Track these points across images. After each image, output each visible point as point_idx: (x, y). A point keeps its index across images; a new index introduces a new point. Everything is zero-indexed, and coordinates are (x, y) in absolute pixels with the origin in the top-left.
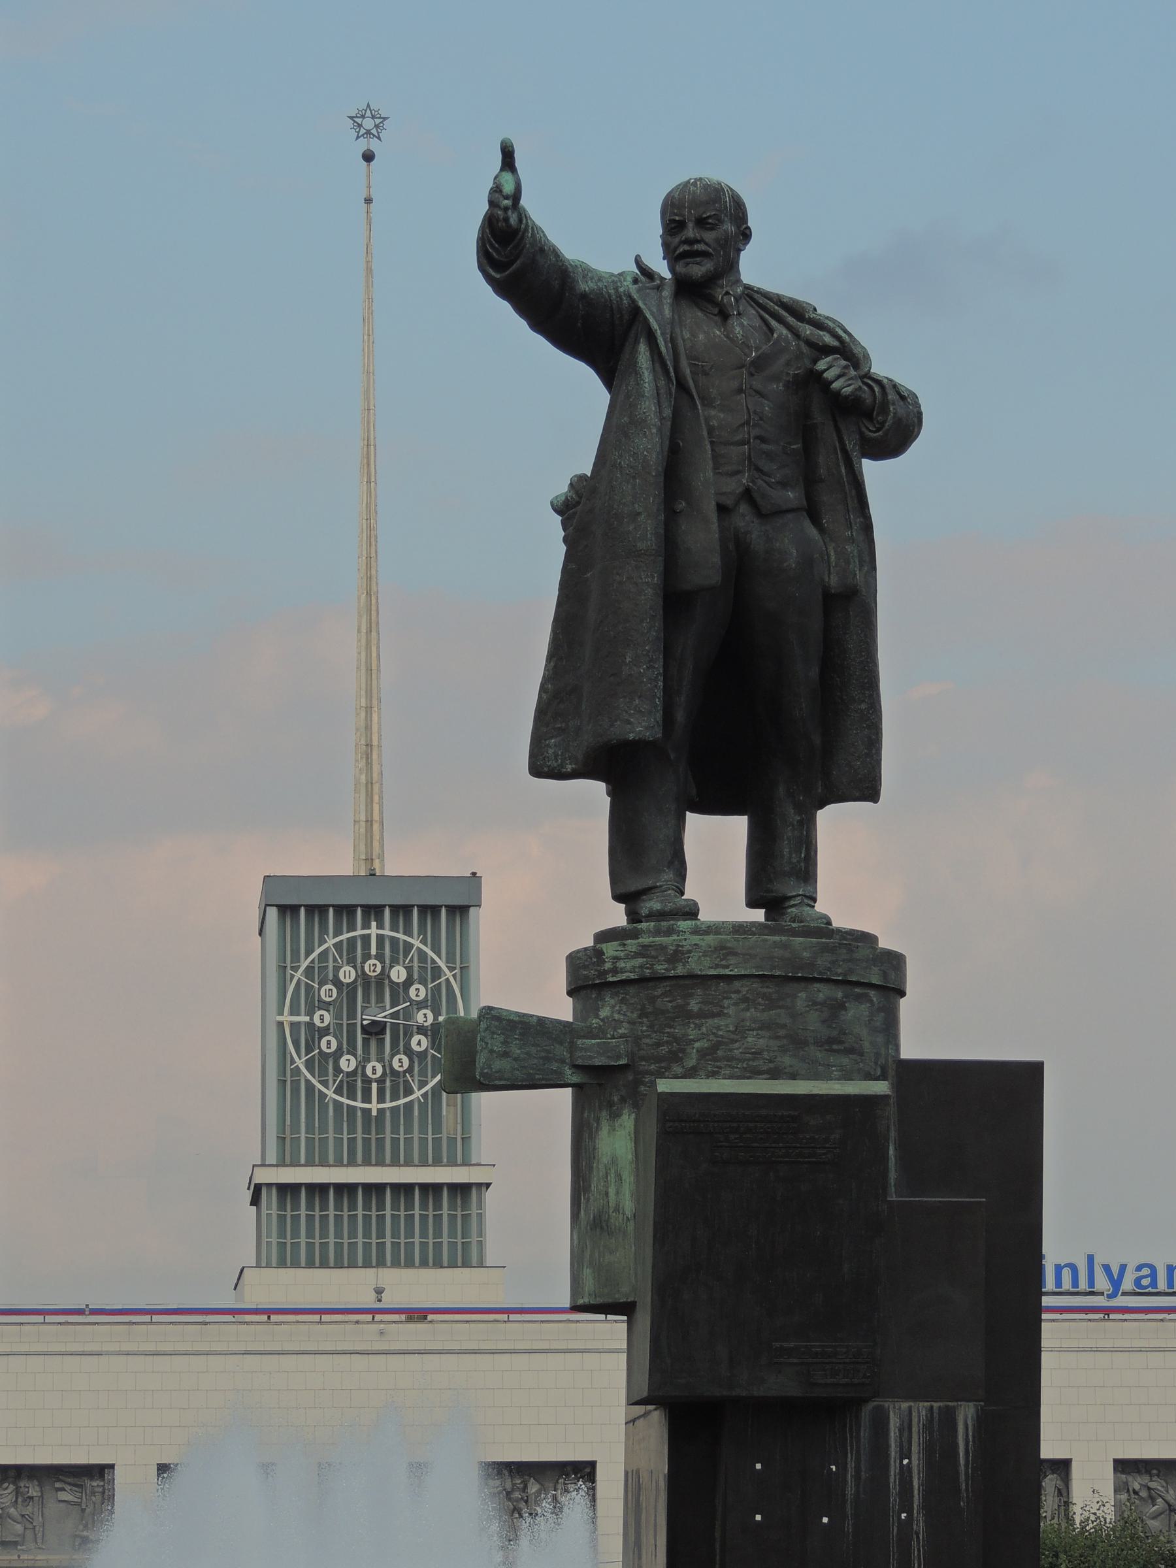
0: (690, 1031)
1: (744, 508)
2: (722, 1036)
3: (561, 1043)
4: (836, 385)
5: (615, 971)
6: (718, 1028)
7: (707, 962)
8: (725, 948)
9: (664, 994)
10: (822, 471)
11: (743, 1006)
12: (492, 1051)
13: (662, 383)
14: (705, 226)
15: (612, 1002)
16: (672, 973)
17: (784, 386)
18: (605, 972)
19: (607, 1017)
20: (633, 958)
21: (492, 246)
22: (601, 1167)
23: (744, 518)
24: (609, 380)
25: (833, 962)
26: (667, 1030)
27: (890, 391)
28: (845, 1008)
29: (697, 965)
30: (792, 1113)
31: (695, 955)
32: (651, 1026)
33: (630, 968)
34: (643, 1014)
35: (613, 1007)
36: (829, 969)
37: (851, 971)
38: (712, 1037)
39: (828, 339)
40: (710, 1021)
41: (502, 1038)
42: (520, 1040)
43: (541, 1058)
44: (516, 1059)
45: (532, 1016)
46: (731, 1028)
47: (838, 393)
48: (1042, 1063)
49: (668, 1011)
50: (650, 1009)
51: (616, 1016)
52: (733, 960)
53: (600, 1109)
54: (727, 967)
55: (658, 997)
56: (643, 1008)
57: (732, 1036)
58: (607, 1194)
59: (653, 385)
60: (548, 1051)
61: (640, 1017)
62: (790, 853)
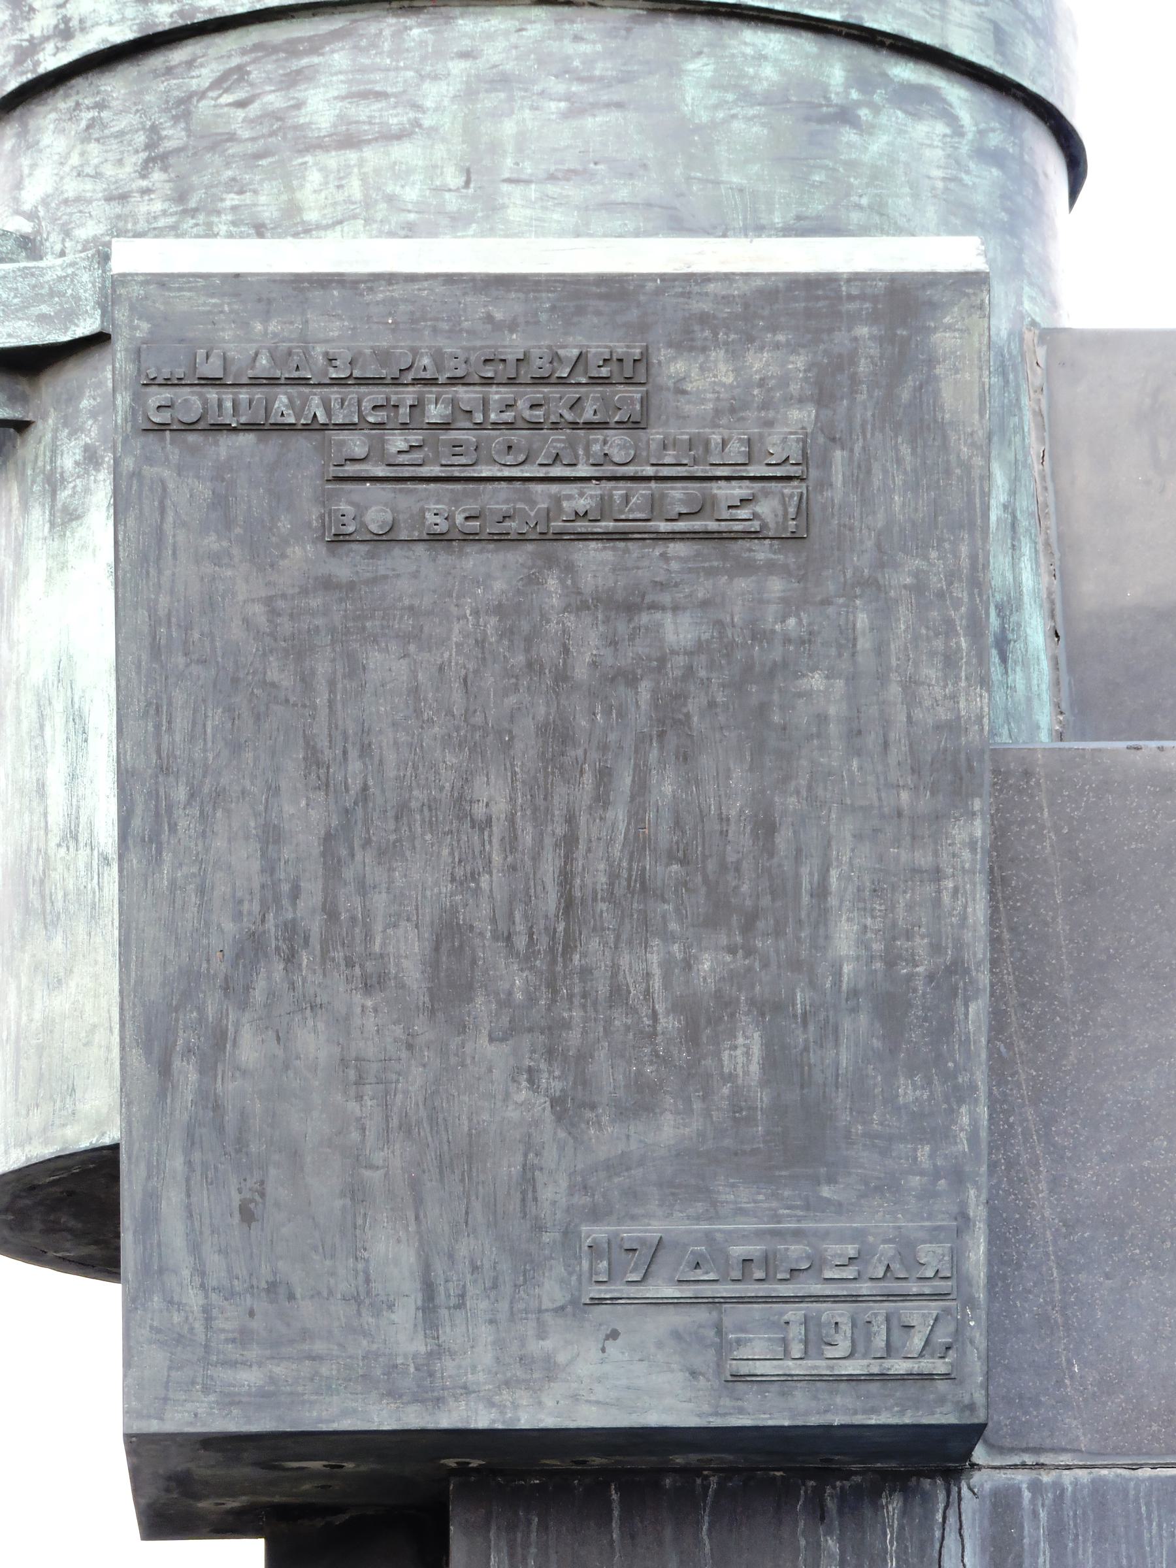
9: (220, 83)
11: (490, 101)
26: (232, 199)
30: (620, 349)
34: (156, 157)
46: (453, 178)
50: (174, 136)
51: (72, 188)
55: (202, 95)
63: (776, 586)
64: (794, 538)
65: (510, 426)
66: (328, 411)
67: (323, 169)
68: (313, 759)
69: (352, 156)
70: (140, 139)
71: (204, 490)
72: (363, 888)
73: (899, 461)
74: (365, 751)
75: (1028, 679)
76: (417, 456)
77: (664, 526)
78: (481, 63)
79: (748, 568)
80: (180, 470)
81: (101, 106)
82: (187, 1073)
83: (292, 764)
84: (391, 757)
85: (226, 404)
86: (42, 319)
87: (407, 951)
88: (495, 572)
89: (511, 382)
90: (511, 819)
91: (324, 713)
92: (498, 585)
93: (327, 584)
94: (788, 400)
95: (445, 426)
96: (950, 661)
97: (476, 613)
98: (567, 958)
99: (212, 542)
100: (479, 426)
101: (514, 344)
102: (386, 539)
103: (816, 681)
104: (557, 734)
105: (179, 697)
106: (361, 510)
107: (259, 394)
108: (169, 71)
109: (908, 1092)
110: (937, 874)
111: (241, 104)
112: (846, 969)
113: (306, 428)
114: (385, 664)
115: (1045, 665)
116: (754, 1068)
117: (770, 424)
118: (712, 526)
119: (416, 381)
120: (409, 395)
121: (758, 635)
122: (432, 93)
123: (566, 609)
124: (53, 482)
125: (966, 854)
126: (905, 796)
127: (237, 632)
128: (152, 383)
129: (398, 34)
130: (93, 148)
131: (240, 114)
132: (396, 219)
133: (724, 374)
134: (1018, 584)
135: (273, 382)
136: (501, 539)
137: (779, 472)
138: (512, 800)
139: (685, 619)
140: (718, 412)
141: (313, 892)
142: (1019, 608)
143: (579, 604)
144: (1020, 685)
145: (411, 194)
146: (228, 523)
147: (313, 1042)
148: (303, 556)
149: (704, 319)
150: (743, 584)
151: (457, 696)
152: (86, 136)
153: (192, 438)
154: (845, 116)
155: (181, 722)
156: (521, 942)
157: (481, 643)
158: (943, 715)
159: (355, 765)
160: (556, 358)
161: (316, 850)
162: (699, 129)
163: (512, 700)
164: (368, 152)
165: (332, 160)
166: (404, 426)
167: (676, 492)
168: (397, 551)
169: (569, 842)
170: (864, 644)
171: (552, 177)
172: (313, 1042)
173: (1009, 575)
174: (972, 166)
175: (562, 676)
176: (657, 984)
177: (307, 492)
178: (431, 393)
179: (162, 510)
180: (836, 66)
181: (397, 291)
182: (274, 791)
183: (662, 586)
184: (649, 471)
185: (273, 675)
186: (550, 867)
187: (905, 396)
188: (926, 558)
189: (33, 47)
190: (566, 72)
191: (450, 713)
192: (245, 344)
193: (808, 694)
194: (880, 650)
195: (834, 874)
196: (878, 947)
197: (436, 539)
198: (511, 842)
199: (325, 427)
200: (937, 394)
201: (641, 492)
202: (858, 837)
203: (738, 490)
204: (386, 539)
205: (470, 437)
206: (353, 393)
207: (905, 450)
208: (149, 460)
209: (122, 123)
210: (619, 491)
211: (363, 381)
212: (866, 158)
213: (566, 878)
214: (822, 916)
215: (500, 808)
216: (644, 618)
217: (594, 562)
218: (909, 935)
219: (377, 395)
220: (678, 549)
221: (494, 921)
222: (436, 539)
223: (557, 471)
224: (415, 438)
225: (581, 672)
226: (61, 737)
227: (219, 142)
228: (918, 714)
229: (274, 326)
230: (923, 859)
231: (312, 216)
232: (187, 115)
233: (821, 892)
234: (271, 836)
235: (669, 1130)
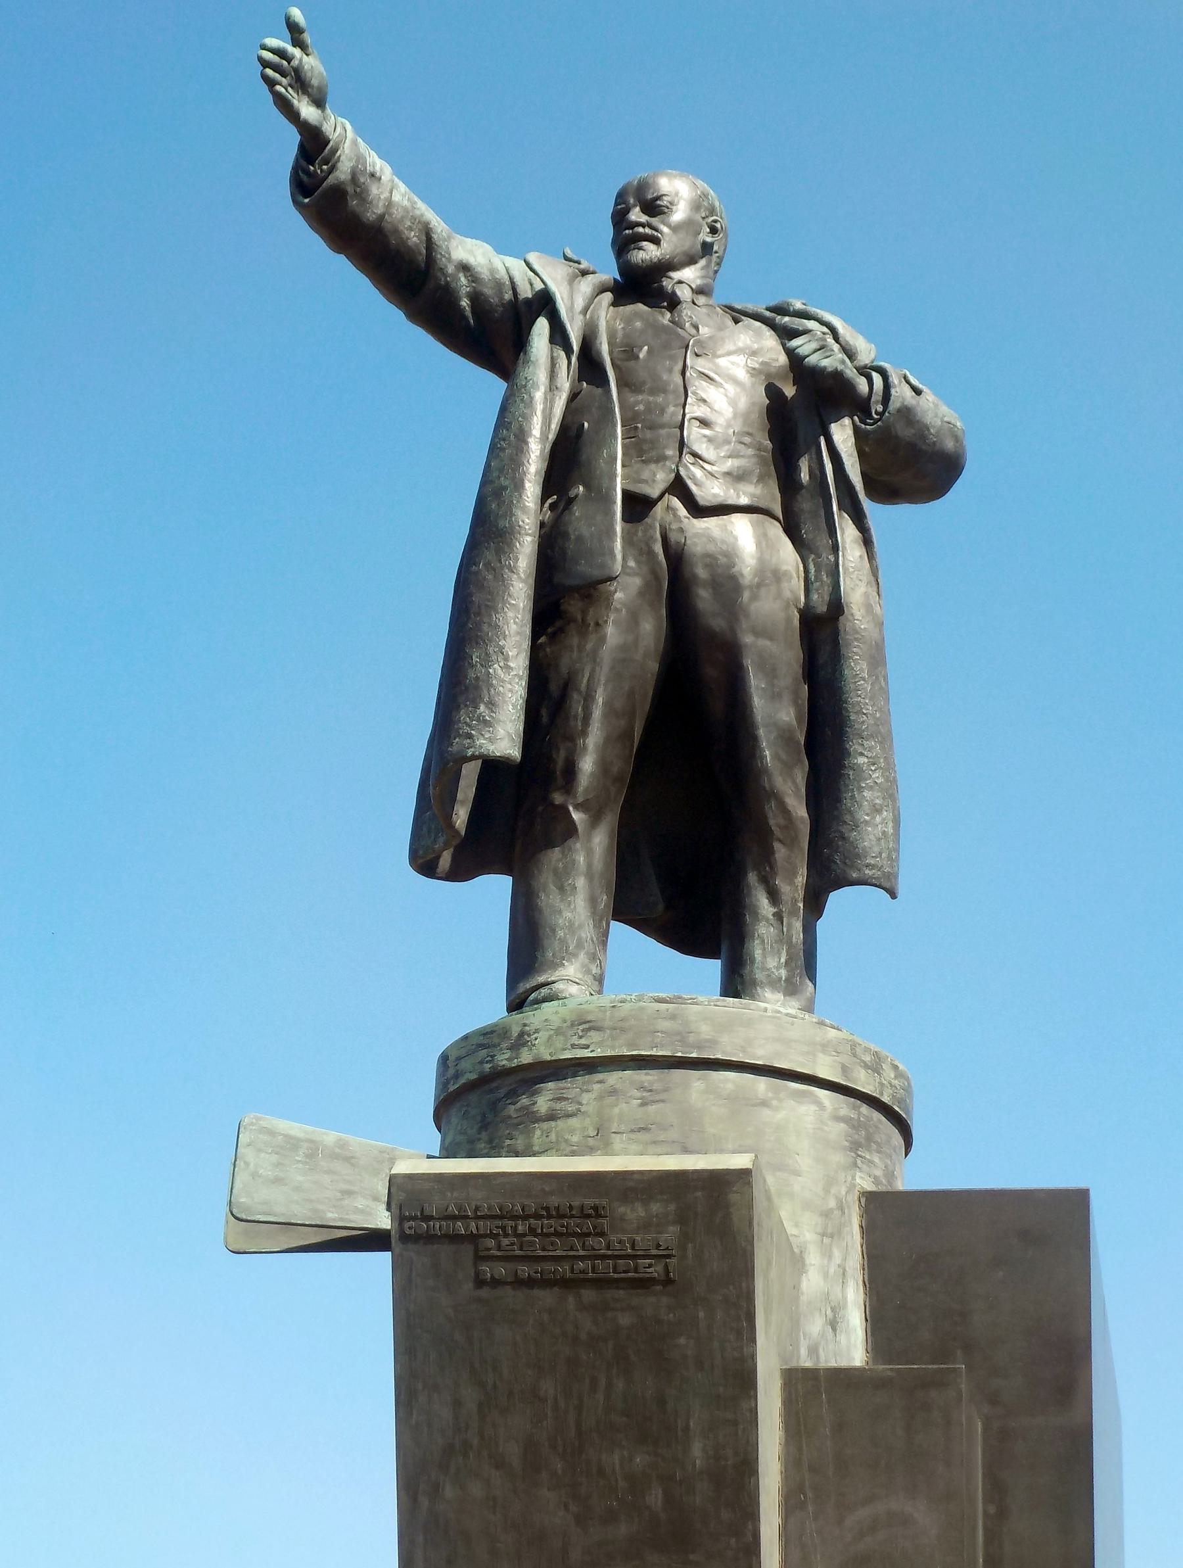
7: (559, 1042)
12: (254, 1175)
16: (515, 1063)
26: (508, 1142)
31: (542, 1036)
44: (297, 1189)
46: (592, 1133)
48: (1071, 1208)
52: (595, 1036)
54: (587, 1047)
69: (553, 1123)
70: (479, 1118)
82: (424, 1502)
87: (513, 1452)
88: (546, 1297)
90: (556, 1399)
101: (554, 1201)
102: (496, 1283)
103: (682, 1341)
108: (491, 1091)
109: (726, 1515)
110: (735, 1423)
112: (698, 1462)
116: (659, 1502)
122: (585, 1098)
126: (721, 1390)
132: (569, 1149)
133: (641, 1212)
134: (845, 1298)
142: (845, 1306)
145: (575, 1139)
147: (476, 1489)
154: (764, 1103)
160: (571, 1207)
164: (559, 1122)
165: (545, 1125)
171: (632, 1131)
172: (476, 1489)
173: (840, 1295)
174: (830, 1123)
176: (617, 1467)
179: (411, 1270)
190: (642, 1088)
196: (711, 1453)
216: (609, 1314)
225: (583, 1336)
229: (455, 1194)
231: (536, 1148)
233: (687, 1429)
234: (457, 1403)
235: (623, 1529)
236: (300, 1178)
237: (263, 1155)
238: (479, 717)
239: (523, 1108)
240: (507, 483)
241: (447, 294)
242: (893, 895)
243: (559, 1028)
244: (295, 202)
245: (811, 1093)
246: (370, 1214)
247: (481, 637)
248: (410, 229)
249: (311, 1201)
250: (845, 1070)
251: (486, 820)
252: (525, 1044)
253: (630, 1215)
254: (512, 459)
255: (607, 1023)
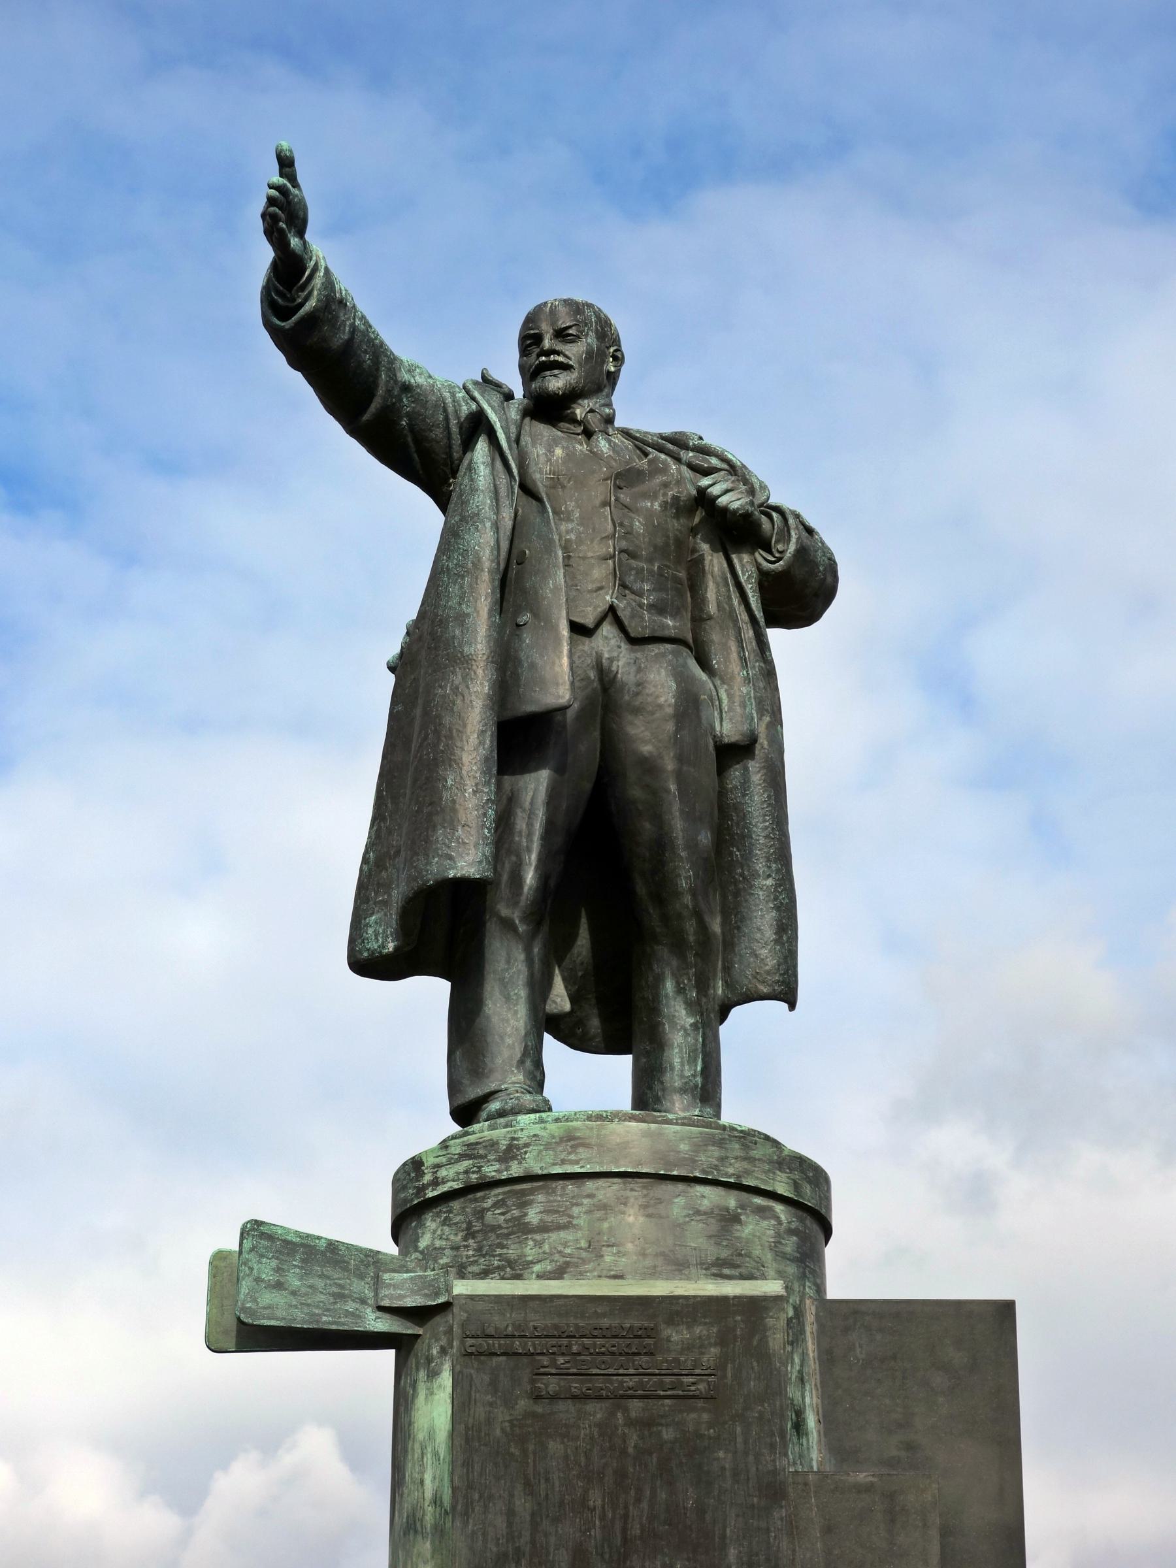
0: (528, 1251)
1: (607, 629)
2: (570, 1255)
3: (362, 1277)
4: (723, 501)
5: (435, 1183)
6: (565, 1245)
7: (549, 1157)
8: (574, 1138)
9: (496, 1205)
10: (712, 608)
11: (599, 1214)
12: (258, 1280)
13: (503, 479)
14: (567, 367)
15: (433, 1225)
16: (504, 1175)
17: (660, 506)
18: (424, 1188)
19: (427, 1247)
20: (458, 1161)
21: (278, 293)
22: (417, 1446)
23: (607, 641)
24: (442, 502)
25: (722, 1159)
26: (499, 1251)
27: (791, 521)
28: (739, 1221)
29: (534, 1163)
30: (646, 1324)
31: (533, 1151)
32: (479, 1249)
33: (452, 1177)
34: (470, 1234)
35: (434, 1232)
36: (716, 1168)
37: (748, 1173)
38: (557, 1257)
39: (714, 461)
40: (554, 1236)
41: (274, 1263)
42: (301, 1268)
43: (333, 1295)
44: (294, 1293)
45: (319, 1238)
46: (583, 1244)
47: (725, 510)
49: (500, 1227)
50: (477, 1226)
51: (438, 1243)
52: (583, 1153)
53: (417, 1370)
54: (577, 1162)
55: (488, 1210)
56: (469, 1224)
57: (584, 1255)
58: (422, 1482)
59: (489, 479)
60: (341, 1287)
61: (465, 1239)
62: (682, 1065)
63: (705, 1417)
64: (712, 1398)
65: (603, 1354)
66: (535, 1348)
67: (534, 1240)
68: (527, 1484)
69: (546, 1235)
70: (464, 1226)
71: (487, 1378)
72: (546, 1535)
73: (752, 1368)
74: (547, 1480)
75: (808, 1440)
76: (567, 1365)
77: (662, 1393)
78: (595, 1200)
79: (693, 1409)
80: (478, 1370)
81: (450, 1212)
83: (519, 1487)
84: (557, 1483)
85: (496, 1344)
86: (426, 1295)
88: (597, 1411)
89: (604, 1337)
90: (603, 1507)
91: (532, 1464)
92: (599, 1416)
93: (534, 1415)
94: (710, 1345)
95: (579, 1354)
96: (772, 1446)
97: (590, 1426)
98: (625, 1562)
99: (489, 1398)
100: (591, 1354)
102: (554, 1398)
103: (721, 1454)
104: (621, 1474)
105: (476, 1458)
106: (547, 1386)
107: (508, 1341)
108: (476, 1200)
110: (768, 1530)
111: (502, 1214)
113: (526, 1354)
114: (554, 1446)
115: (815, 1434)
117: (703, 1353)
118: (681, 1393)
119: (567, 1337)
120: (565, 1341)
121: (702, 1436)
123: (625, 1425)
124: (429, 1360)
125: (779, 1523)
127: (498, 1432)
128: (467, 1337)
129: (563, 1188)
130: (446, 1229)
131: (503, 1218)
135: (513, 1336)
136: (600, 1398)
137: (706, 1372)
138: (603, 1500)
139: (671, 1430)
140: (682, 1349)
141: (526, 1535)
143: (630, 1423)
144: (805, 1443)
146: (496, 1391)
148: (523, 1404)
149: (678, 1313)
150: (693, 1415)
151: (583, 1459)
152: (444, 1223)
153: (482, 1358)
155: (477, 1467)
156: (607, 1556)
157: (592, 1438)
158: (770, 1467)
159: (543, 1486)
161: (528, 1518)
162: (679, 1225)
163: (604, 1461)
165: (538, 1237)
166: (563, 1354)
167: (667, 1379)
168: (560, 1402)
169: (626, 1516)
170: (739, 1440)
175: (624, 1452)
177: (526, 1379)
178: (573, 1341)
180: (731, 1200)
181: (561, 1302)
182: (512, 1496)
183: (662, 1417)
184: (657, 1372)
185: (513, 1450)
186: (618, 1526)
187: (755, 1343)
188: (763, 1405)
189: (424, 1188)
191: (580, 1465)
192: (502, 1321)
193: (718, 1459)
194: (746, 1442)
195: (728, 1531)
197: (574, 1397)
198: (603, 1517)
199: (532, 1354)
200: (767, 1342)
201: (655, 1379)
202: (737, 1516)
203: (691, 1379)
204: (554, 1398)
205: (588, 1358)
206: (543, 1341)
207: (755, 1364)
208: (466, 1367)
209: (457, 1219)
210: (646, 1379)
211: (547, 1336)
212: (744, 1235)
213: (624, 1530)
214: (723, 1547)
215: (599, 1502)
217: (635, 1406)
218: (757, 1555)
219: (554, 1341)
220: (667, 1401)
221: (596, 1547)
222: (574, 1397)
223: (621, 1371)
224: (567, 1358)
225: (631, 1450)
226: (430, 1462)
227: (494, 1228)
228: (760, 1467)
230: (763, 1525)
232: (482, 1218)
233: (723, 1537)
234: (511, 1513)
236: (298, 1283)
237: (264, 1260)
238: (458, 839)
239: (513, 1219)
240: (469, 610)
241: (389, 414)
242: (792, 1006)
243: (548, 1144)
244: (267, 324)
245: (770, 1209)
246: (359, 1317)
247: (455, 761)
248: (366, 352)
249: (308, 1305)
250: (796, 1186)
251: (420, 925)
252: (514, 1158)
253: (675, 1338)
254: (471, 586)
255: (593, 1141)
